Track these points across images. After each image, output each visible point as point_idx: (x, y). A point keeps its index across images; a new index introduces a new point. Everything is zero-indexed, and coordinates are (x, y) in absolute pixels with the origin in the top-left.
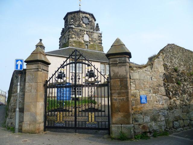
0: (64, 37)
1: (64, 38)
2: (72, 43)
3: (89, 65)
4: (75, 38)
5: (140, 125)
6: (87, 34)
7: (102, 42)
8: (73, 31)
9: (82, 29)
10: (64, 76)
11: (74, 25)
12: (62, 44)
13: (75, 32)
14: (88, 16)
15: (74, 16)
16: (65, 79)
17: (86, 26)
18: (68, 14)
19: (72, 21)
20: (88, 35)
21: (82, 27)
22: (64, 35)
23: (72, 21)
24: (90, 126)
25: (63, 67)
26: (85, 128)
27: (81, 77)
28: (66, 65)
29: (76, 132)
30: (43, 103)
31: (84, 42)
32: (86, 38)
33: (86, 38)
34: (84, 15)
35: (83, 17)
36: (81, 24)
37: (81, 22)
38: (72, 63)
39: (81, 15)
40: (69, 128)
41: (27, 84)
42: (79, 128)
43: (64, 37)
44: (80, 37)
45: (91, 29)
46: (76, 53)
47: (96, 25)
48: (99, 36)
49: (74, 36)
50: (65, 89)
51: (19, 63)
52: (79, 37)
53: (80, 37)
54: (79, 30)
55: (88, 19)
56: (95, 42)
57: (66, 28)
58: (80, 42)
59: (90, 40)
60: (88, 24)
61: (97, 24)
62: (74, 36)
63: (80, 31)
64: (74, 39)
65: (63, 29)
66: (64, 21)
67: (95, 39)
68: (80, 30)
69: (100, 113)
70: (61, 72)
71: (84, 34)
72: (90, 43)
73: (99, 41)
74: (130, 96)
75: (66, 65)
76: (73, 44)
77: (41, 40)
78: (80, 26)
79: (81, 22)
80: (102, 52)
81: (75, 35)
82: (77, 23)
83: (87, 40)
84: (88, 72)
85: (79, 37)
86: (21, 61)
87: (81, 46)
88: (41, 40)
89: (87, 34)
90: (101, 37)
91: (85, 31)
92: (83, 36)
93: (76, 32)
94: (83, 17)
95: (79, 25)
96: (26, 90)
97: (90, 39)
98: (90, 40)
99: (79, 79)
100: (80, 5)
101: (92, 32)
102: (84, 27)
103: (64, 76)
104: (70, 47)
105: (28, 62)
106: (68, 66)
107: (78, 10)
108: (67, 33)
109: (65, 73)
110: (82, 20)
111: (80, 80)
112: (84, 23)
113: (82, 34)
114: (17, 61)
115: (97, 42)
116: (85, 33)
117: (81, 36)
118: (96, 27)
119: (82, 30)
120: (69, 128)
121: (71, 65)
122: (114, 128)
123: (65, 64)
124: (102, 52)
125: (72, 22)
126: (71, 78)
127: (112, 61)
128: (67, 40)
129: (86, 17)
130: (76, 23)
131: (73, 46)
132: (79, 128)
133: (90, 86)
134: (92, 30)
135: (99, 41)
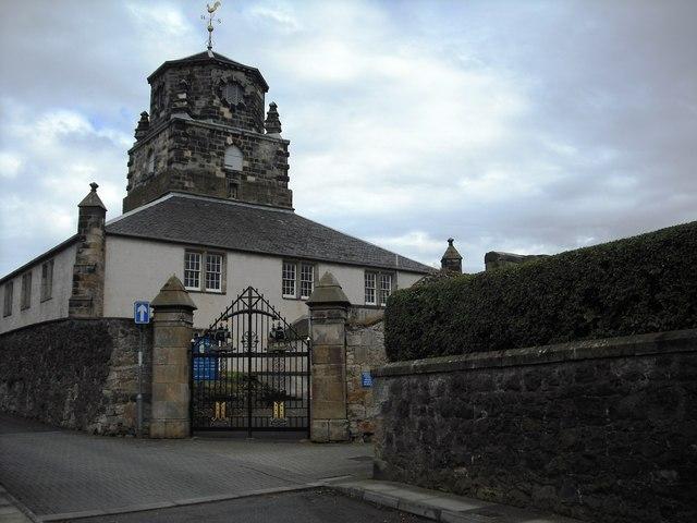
0: (151, 151)
1: (149, 156)
2: (184, 179)
3: (274, 318)
4: (194, 160)
5: (359, 421)
6: (234, 144)
7: (290, 173)
8: (185, 135)
9: (220, 125)
10: (229, 336)
11: (189, 112)
12: (138, 174)
13: (194, 137)
14: (240, 76)
15: (191, 78)
16: (229, 340)
17: (234, 117)
18: (168, 66)
19: (184, 96)
20: (241, 149)
21: (218, 118)
22: (148, 143)
23: (184, 96)
24: (275, 425)
25: (226, 319)
26: (268, 429)
27: (259, 339)
28: (232, 315)
29: (250, 436)
30: (187, 385)
31: (223, 175)
32: (234, 160)
33: (234, 160)
34: (226, 75)
35: (222, 83)
36: (215, 108)
37: (217, 101)
38: (243, 312)
39: (215, 74)
40: (238, 429)
41: (157, 351)
42: (257, 429)
43: (151, 151)
44: (209, 157)
45: (251, 126)
46: (250, 293)
47: (267, 109)
48: (279, 153)
49: (188, 154)
50: (299, 378)
51: (142, 309)
52: (208, 158)
53: (209, 157)
54: (208, 132)
55: (242, 89)
56: (264, 172)
57: (158, 116)
58: (210, 176)
59: (245, 168)
60: (240, 107)
61: (273, 107)
62: (188, 154)
63: (211, 136)
64: (190, 166)
65: (144, 115)
66: (148, 88)
67: (264, 161)
68: (212, 131)
69: (293, 403)
70: (221, 328)
71: (226, 144)
72: (244, 177)
73: (277, 172)
74: (344, 374)
75: (232, 315)
76: (187, 185)
77: (94, 187)
78: (211, 117)
79: (217, 101)
80: (287, 212)
81: (191, 149)
82: (201, 103)
83: (233, 168)
84: (274, 329)
85: (208, 158)
86: (146, 305)
87: (213, 189)
88: (94, 187)
89: (234, 144)
90: (288, 155)
91: (227, 134)
92: (222, 154)
93: (198, 138)
94: (222, 83)
95: (210, 112)
96: (156, 361)
97: (246, 164)
98: (245, 168)
99: (257, 342)
100: (210, 30)
101: (252, 139)
102: (225, 119)
103: (229, 336)
104: (177, 195)
105: (158, 308)
106: (235, 317)
107: (199, 48)
108: (161, 137)
109: (230, 330)
110: (220, 94)
111: (259, 345)
112: (225, 104)
113: (218, 145)
114: (138, 305)
115: (269, 173)
116: (230, 140)
117: (211, 153)
118: (266, 116)
119: (219, 132)
120: (238, 429)
121: (241, 316)
122: (316, 425)
123: (230, 312)
124: (287, 212)
125: (183, 100)
126: (240, 339)
127: (317, 315)
128: (161, 165)
129: (231, 81)
130: (197, 103)
131: (187, 188)
132: (257, 429)
133: (276, 355)
134: (254, 131)
135: (277, 172)
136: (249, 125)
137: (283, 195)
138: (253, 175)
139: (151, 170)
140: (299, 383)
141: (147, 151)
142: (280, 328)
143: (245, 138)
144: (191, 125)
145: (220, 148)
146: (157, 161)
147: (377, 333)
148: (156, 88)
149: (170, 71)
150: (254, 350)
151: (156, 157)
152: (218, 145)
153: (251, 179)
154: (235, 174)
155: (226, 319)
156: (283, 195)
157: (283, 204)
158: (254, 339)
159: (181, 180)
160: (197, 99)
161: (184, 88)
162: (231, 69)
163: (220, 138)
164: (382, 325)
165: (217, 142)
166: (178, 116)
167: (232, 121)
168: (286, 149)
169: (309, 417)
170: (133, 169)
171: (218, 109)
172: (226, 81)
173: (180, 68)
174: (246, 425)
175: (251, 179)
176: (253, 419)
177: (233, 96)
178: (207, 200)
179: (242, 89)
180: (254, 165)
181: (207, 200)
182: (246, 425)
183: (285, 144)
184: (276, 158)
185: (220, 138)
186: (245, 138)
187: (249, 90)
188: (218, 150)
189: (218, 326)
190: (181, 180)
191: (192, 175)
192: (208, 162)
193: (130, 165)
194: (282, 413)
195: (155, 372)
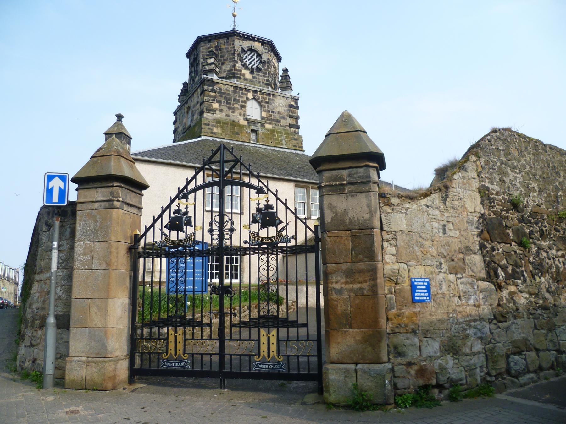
0: (189, 108)
1: (188, 113)
2: (213, 126)
4: (221, 111)
6: (254, 98)
9: (241, 84)
10: (189, 223)
12: (180, 129)
13: (221, 93)
14: (257, 46)
15: (218, 48)
16: (190, 230)
18: (200, 40)
19: (212, 60)
20: (259, 103)
21: (240, 78)
23: (212, 60)
24: (263, 368)
25: (186, 197)
27: (236, 226)
28: (194, 190)
29: (222, 386)
31: (245, 123)
34: (247, 44)
35: (243, 51)
39: (238, 43)
41: (79, 247)
43: (189, 108)
45: (268, 85)
46: (222, 155)
47: (281, 73)
48: (291, 106)
49: (216, 106)
51: (57, 184)
52: (233, 109)
54: (232, 89)
55: (259, 56)
56: (279, 121)
57: (194, 80)
61: (285, 71)
62: (216, 106)
63: (235, 92)
64: (218, 115)
65: (185, 84)
68: (236, 88)
69: (293, 331)
70: (178, 211)
71: (248, 99)
72: (263, 125)
73: (290, 121)
75: (194, 190)
76: (215, 130)
78: (234, 77)
79: (239, 65)
80: (299, 152)
81: (219, 102)
82: (227, 67)
84: (259, 210)
85: (233, 109)
86: (63, 178)
89: (254, 98)
91: (248, 90)
92: (243, 107)
93: (224, 93)
94: (243, 51)
95: (233, 74)
97: (264, 114)
98: (263, 118)
99: (232, 230)
100: (234, 16)
101: (268, 94)
102: (246, 79)
103: (189, 223)
106: (200, 193)
108: (195, 95)
109: (191, 214)
111: (236, 235)
113: (241, 99)
114: (50, 177)
115: (283, 122)
116: (250, 95)
117: (236, 106)
118: (280, 78)
119: (241, 89)
123: (191, 186)
124: (299, 152)
126: (207, 227)
129: (251, 50)
130: (223, 67)
131: (215, 133)
133: (264, 251)
134: (270, 88)
135: (290, 121)
136: (266, 84)
137: (295, 139)
138: (270, 124)
139: (189, 123)
140: (419, 294)
141: (186, 109)
142: (268, 207)
143: (263, 93)
144: (218, 83)
145: (242, 102)
146: (193, 115)
147: (431, 211)
148: (192, 60)
149: (202, 44)
150: (227, 243)
151: (192, 112)
152: (241, 99)
153: (268, 126)
154: (255, 122)
155: (186, 197)
156: (295, 139)
157: (296, 146)
158: (228, 226)
159: (210, 127)
160: (223, 64)
161: (211, 54)
162: (250, 40)
163: (242, 93)
164: (251, 189)
165: (239, 97)
166: (210, 77)
167: (252, 81)
168: (296, 103)
169: (319, 356)
170: (177, 126)
171: (241, 71)
172: (246, 49)
173: (210, 41)
174: (216, 368)
175: (268, 126)
176: (227, 358)
177: (251, 60)
178: (232, 142)
179: (259, 56)
180: (271, 116)
181: (232, 142)
182: (216, 368)
183: (296, 100)
184: (289, 110)
185: (242, 93)
186: (263, 93)
187: (265, 57)
188: (240, 103)
189: (174, 207)
190: (210, 127)
191: (218, 122)
192: (233, 112)
193: (175, 123)
194: (273, 348)
195: (75, 280)
